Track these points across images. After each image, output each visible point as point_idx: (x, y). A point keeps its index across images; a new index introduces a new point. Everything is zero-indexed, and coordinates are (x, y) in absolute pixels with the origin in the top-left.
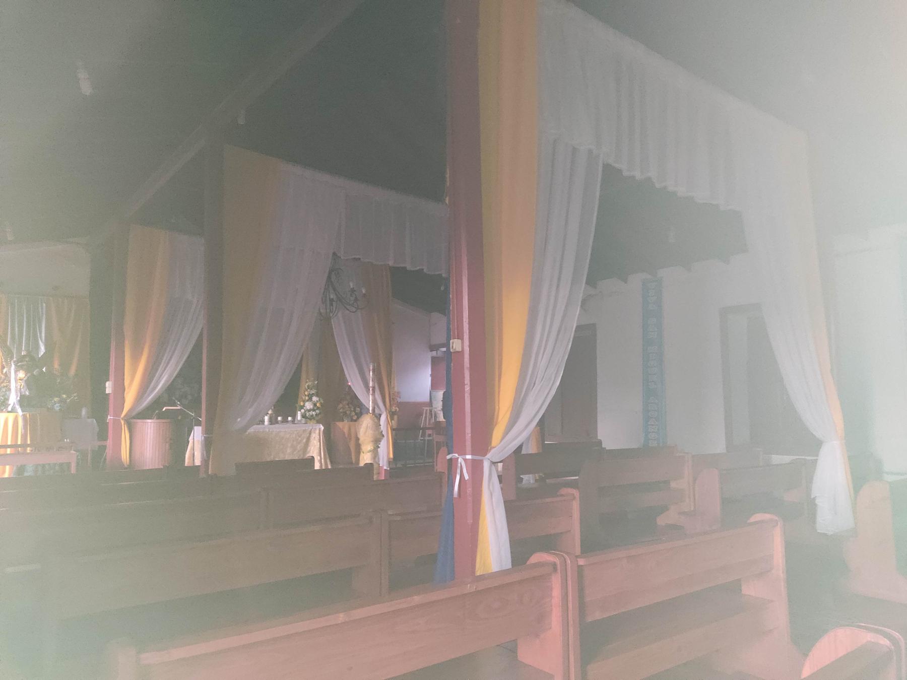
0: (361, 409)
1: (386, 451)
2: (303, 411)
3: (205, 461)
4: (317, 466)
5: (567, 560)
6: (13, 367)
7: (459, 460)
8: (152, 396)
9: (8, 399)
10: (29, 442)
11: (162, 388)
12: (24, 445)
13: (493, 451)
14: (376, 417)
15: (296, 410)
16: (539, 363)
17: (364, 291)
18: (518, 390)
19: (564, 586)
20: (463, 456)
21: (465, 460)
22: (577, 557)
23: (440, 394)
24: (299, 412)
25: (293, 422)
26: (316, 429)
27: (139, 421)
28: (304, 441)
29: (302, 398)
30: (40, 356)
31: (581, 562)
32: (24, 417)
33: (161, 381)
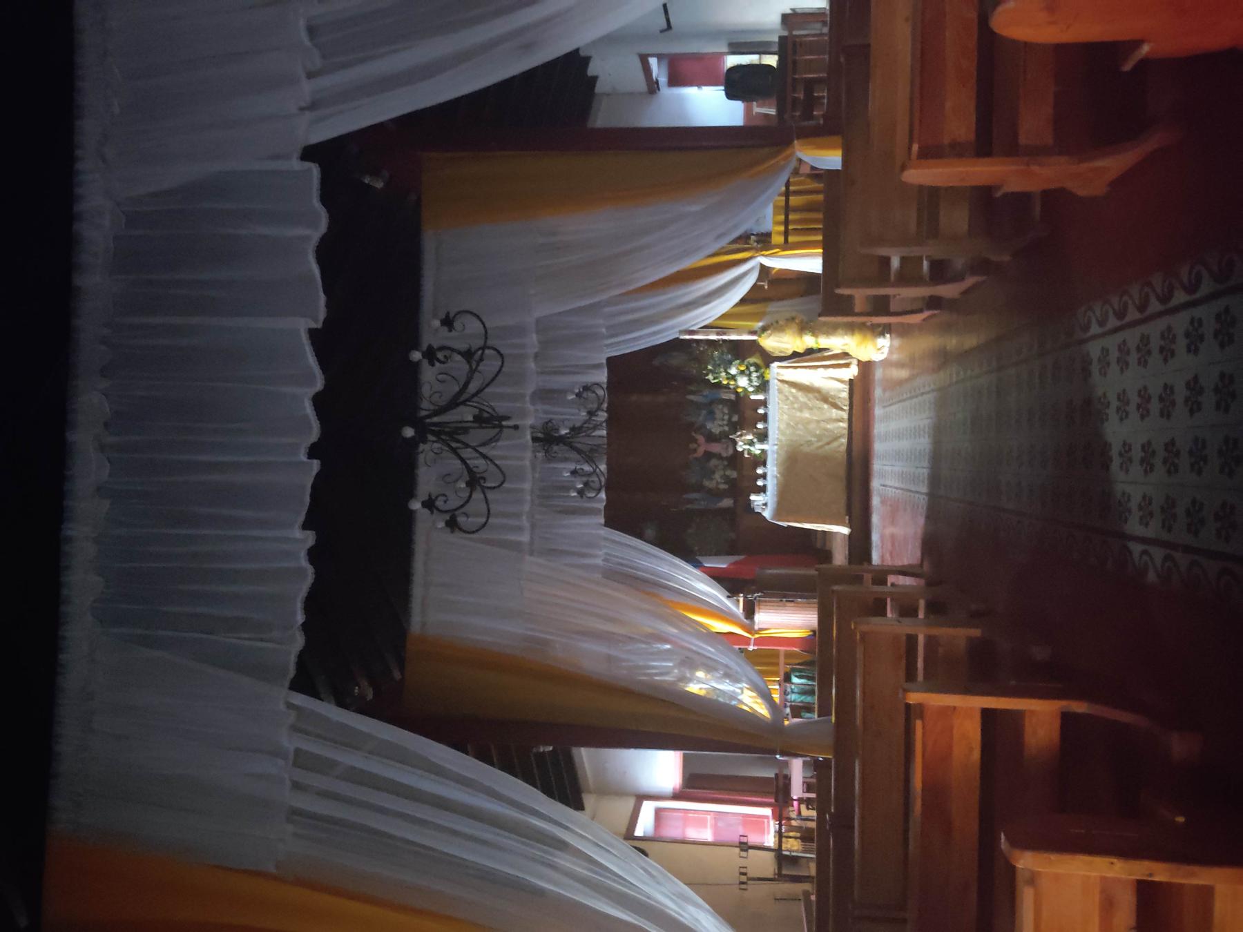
0: (753, 235)
28: (794, 391)
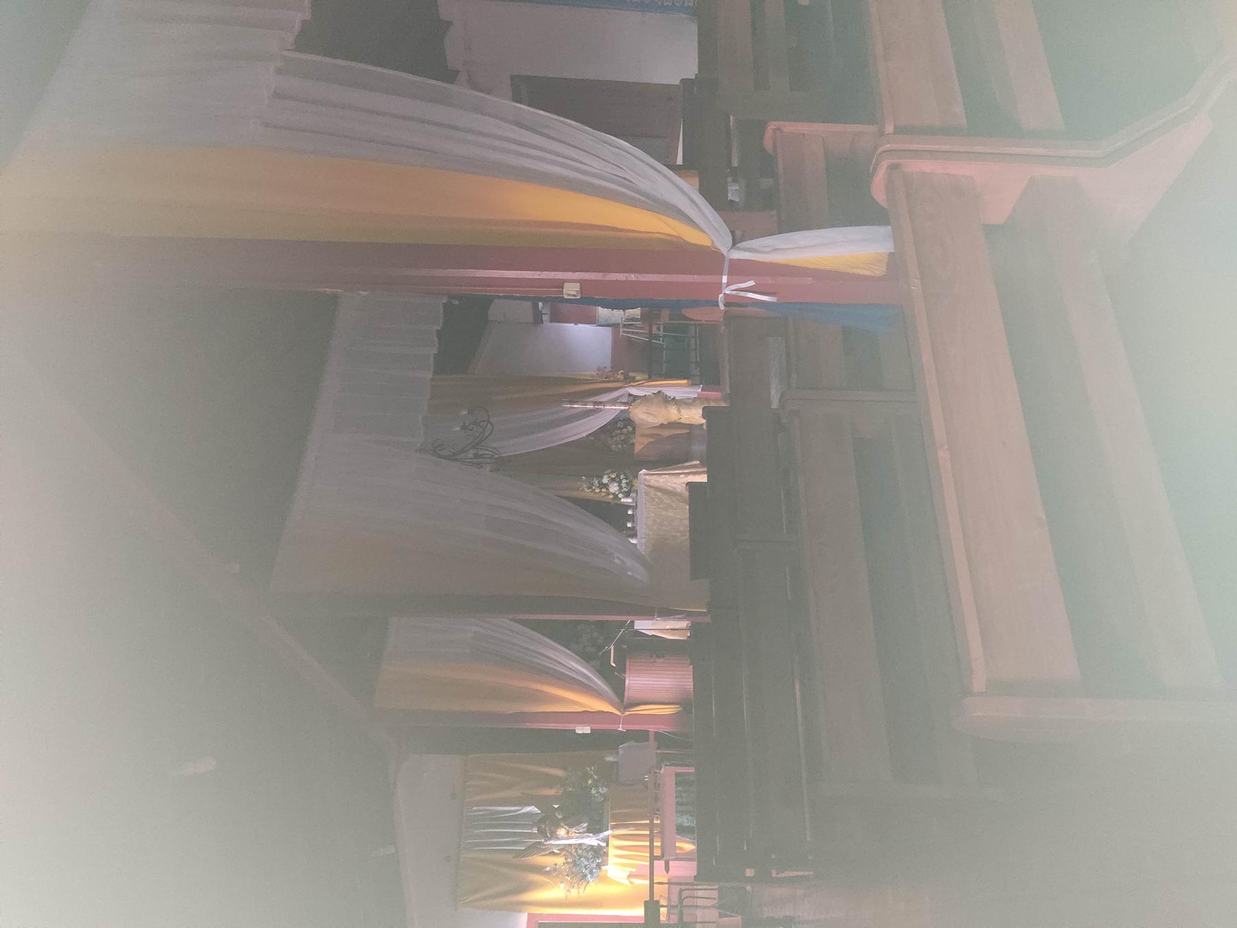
1: (678, 389)
2: (620, 496)
3: (688, 615)
4: (703, 478)
5: (885, 150)
6: (551, 842)
7: (728, 292)
8: (596, 680)
9: (592, 846)
10: (648, 822)
11: (584, 667)
12: (651, 827)
13: (718, 245)
14: (634, 400)
15: (619, 504)
16: (597, 171)
17: (465, 412)
18: (633, 203)
19: (916, 154)
20: (724, 286)
21: (728, 284)
22: (882, 134)
23: (602, 312)
24: (622, 500)
25: (634, 508)
26: (645, 479)
27: (626, 694)
28: (659, 494)
29: (604, 496)
30: (539, 812)
31: (889, 129)
32: (613, 828)
33: (577, 669)
